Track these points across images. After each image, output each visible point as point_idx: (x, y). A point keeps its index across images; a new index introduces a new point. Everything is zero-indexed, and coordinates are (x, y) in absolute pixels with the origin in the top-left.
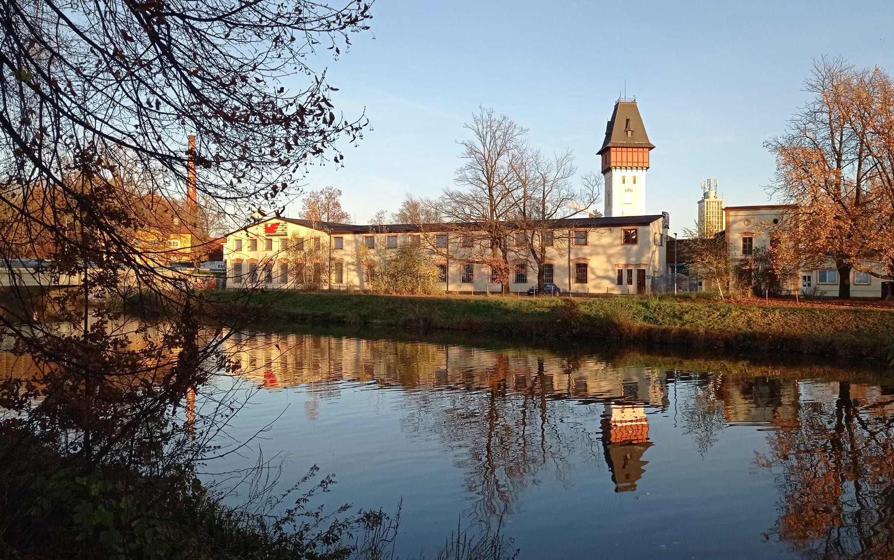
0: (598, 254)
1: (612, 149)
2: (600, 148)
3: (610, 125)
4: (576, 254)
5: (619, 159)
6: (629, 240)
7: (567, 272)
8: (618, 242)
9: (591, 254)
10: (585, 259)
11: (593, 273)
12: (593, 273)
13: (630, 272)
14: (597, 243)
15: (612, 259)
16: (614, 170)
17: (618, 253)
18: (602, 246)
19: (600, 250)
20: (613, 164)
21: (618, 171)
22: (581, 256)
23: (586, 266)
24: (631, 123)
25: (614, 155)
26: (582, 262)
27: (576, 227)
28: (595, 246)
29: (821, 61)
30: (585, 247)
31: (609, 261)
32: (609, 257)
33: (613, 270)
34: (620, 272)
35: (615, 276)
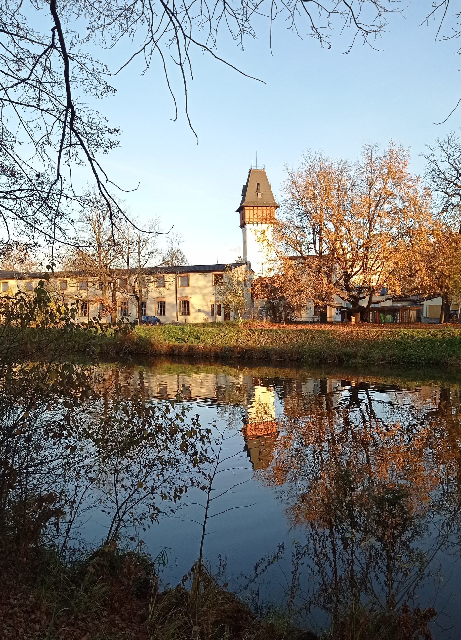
0: (196, 293)
1: (246, 208)
2: (238, 207)
3: (245, 188)
4: (181, 294)
5: (252, 216)
6: (218, 281)
7: (176, 308)
8: (211, 284)
9: (191, 294)
10: (187, 297)
11: (193, 308)
12: (193, 308)
13: (219, 306)
14: (195, 285)
15: (206, 297)
16: (247, 225)
17: (210, 293)
18: (199, 288)
19: (198, 290)
20: (247, 220)
21: (251, 225)
22: (184, 295)
23: (188, 302)
24: (260, 187)
25: (248, 213)
26: (185, 299)
27: (180, 273)
28: (194, 287)
29: (307, 154)
30: (187, 288)
31: (204, 299)
32: (204, 295)
33: (207, 305)
34: (212, 306)
35: (209, 309)
